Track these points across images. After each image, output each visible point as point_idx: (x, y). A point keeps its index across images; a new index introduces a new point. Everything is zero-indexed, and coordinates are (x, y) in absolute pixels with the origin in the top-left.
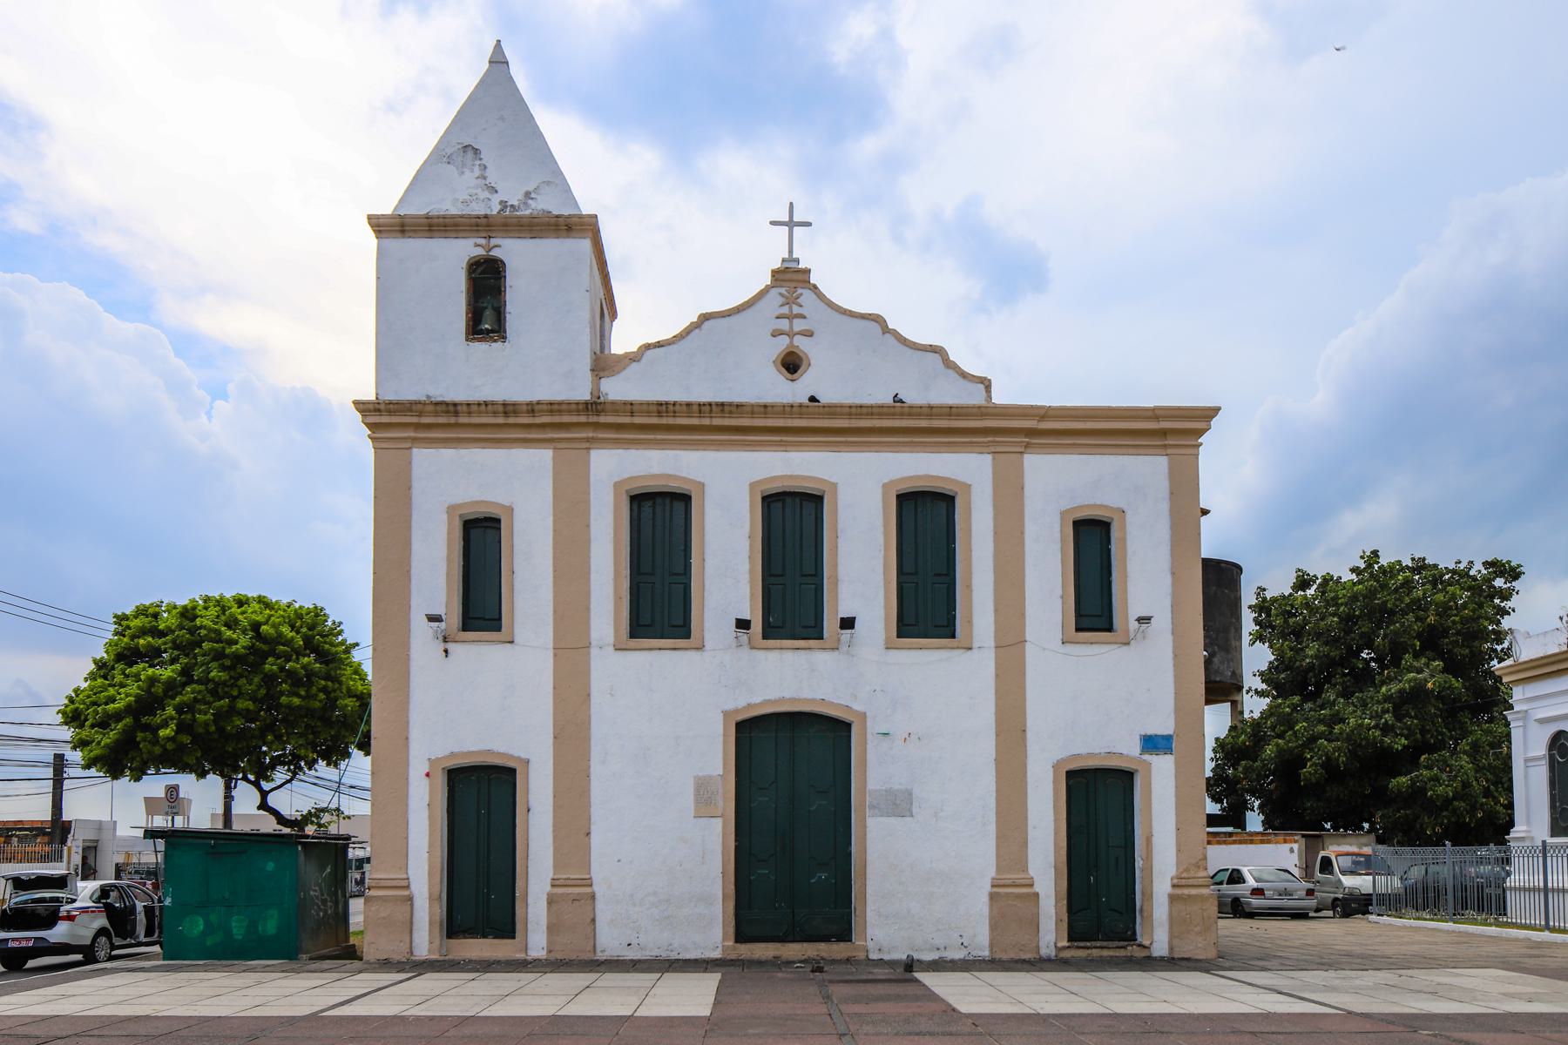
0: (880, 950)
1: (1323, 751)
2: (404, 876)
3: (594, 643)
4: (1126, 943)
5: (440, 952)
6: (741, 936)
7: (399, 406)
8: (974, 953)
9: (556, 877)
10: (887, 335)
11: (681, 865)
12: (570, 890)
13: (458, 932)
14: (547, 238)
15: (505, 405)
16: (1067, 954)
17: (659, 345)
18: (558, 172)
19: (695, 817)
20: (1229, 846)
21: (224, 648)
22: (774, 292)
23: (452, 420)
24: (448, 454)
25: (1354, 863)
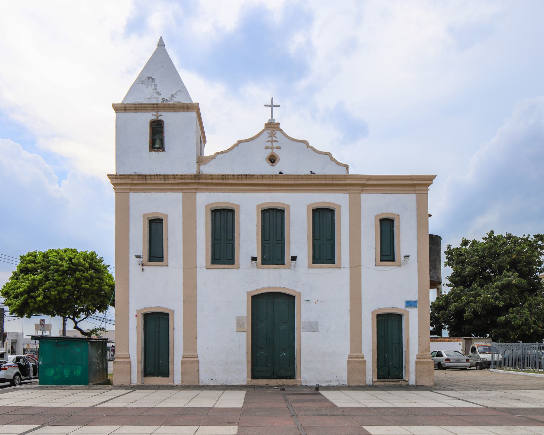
0: (306, 382)
2: (128, 354)
3: (198, 266)
4: (399, 380)
5: (141, 382)
6: (254, 376)
8: (341, 383)
11: (231, 350)
13: (148, 375)
14: (180, 112)
16: (377, 384)
17: (222, 153)
19: (236, 332)
21: (59, 268)
22: (266, 132)
23: (145, 182)
24: (143, 195)
25: (484, 349)
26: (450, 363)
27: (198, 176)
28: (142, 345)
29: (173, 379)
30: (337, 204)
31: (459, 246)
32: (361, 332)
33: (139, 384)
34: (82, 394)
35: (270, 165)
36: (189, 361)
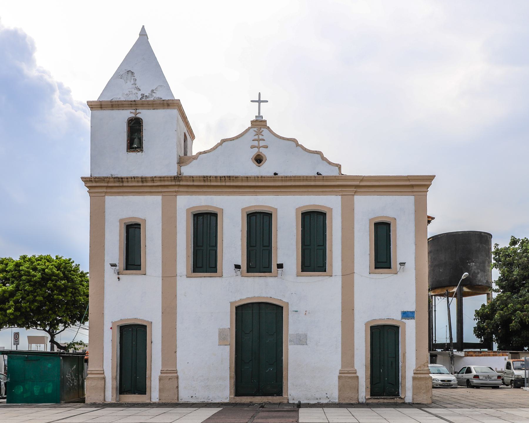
1: (519, 316)
2: (176, 369)
5: (116, 400)
6: (238, 393)
7: (99, 179)
8: (332, 401)
9: (163, 369)
10: (298, 147)
12: (168, 375)
13: (124, 392)
14: (159, 109)
15: (142, 178)
16: (370, 401)
17: (205, 152)
18: (166, 82)
20: (480, 357)
21: (31, 279)
22: (252, 130)
24: (119, 198)
25: (522, 365)
26: (479, 380)
27: (178, 178)
28: (117, 359)
29: (150, 396)
30: (328, 207)
31: (508, 246)
32: (354, 345)
33: (114, 402)
34: (47, 411)
35: (256, 166)
36: (167, 376)
